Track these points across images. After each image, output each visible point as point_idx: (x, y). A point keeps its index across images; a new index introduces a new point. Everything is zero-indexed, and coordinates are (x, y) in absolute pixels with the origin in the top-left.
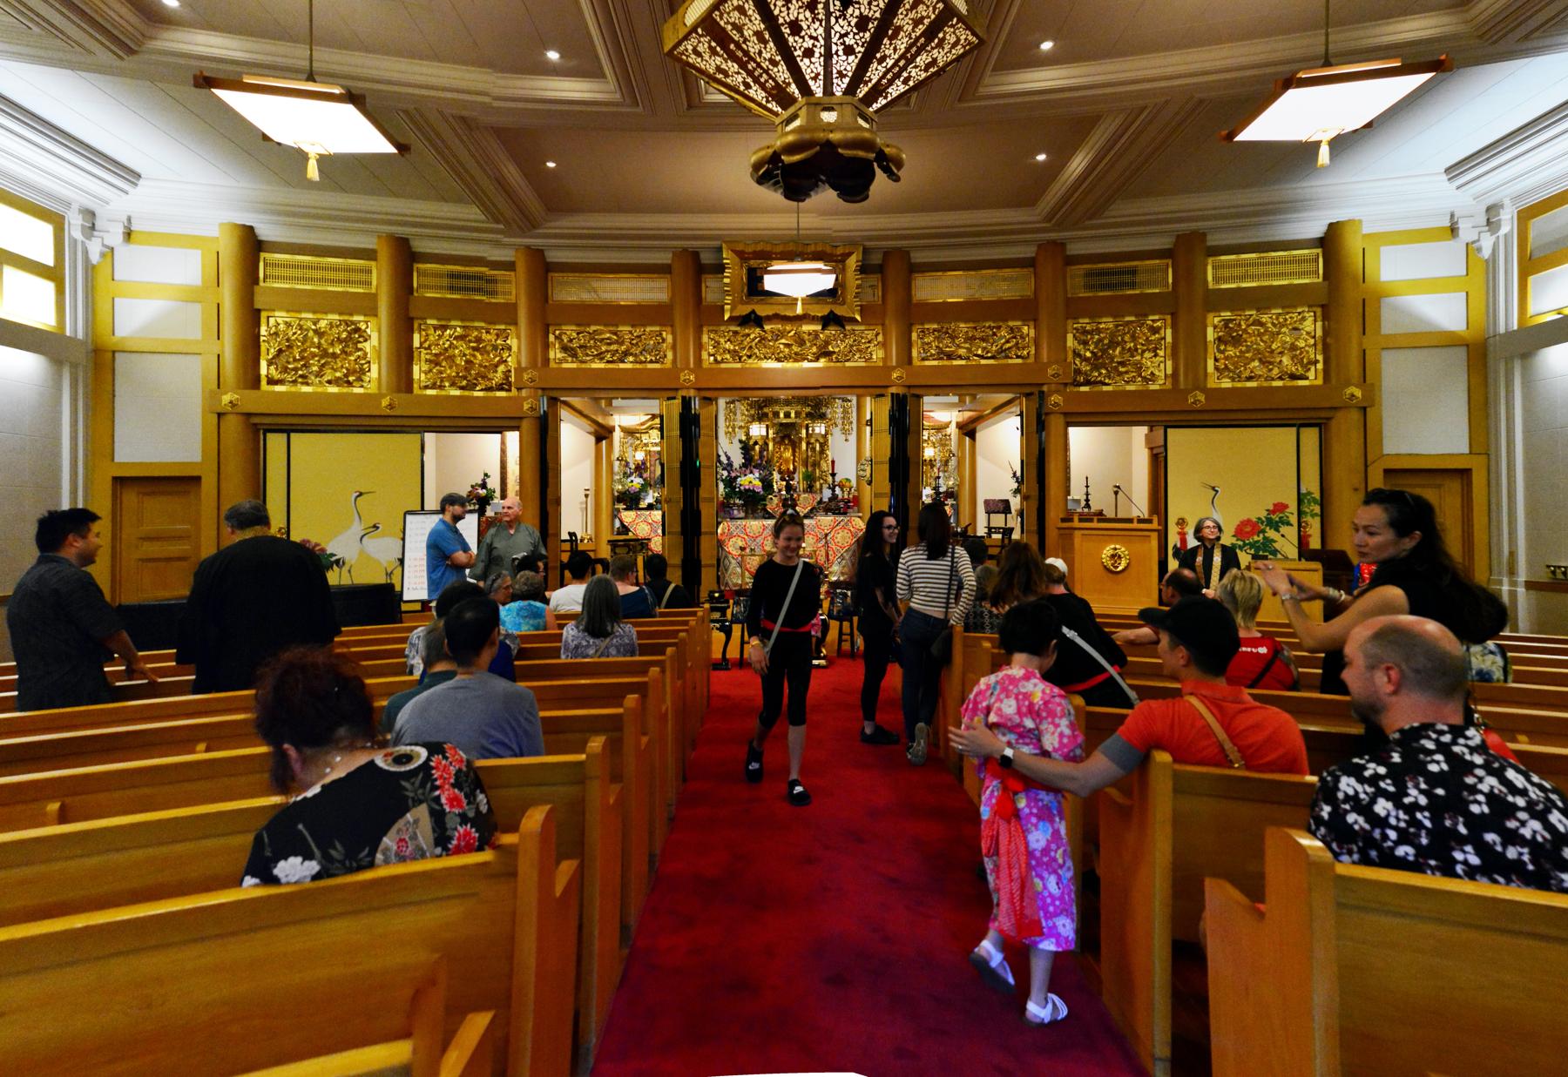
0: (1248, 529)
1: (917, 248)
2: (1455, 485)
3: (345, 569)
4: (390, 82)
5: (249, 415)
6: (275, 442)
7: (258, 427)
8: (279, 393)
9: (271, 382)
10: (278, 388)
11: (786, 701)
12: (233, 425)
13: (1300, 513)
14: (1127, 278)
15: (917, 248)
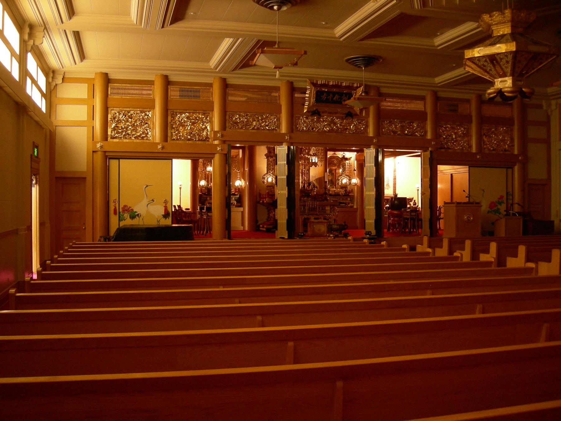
1: (385, 87)
2: (229, 91)
3: (141, 218)
4: (453, 78)
5: (105, 152)
6: (114, 164)
7: (108, 157)
9: (113, 138)
10: (115, 140)
11: (177, 225)
12: (99, 157)
13: (507, 199)
14: (185, 93)
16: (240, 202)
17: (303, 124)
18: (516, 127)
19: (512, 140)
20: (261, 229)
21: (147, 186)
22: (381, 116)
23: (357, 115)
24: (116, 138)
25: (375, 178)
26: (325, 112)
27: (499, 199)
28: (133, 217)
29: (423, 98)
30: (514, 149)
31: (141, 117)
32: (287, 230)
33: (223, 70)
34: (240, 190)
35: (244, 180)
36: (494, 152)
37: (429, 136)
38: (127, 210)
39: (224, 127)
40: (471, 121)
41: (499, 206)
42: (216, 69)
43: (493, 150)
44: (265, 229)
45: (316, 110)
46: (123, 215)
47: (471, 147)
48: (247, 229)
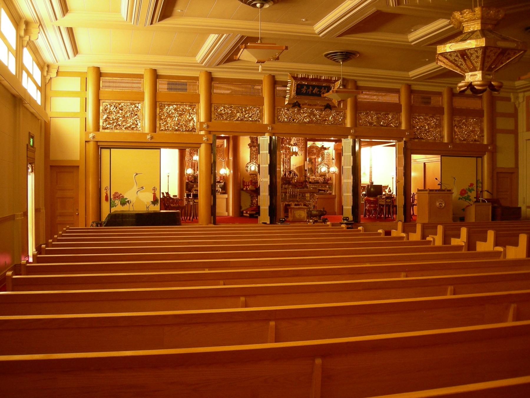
0: (463, 192)
3: (131, 204)
5: (97, 142)
6: (105, 153)
7: (99, 147)
8: (105, 135)
9: (104, 128)
10: (106, 131)
12: (91, 147)
13: (477, 187)
14: (183, 87)
15: (360, 80)
16: (225, 189)
17: (284, 115)
18: (485, 119)
19: (482, 131)
20: (245, 215)
21: (137, 174)
22: (357, 108)
23: (335, 107)
24: (107, 128)
25: (352, 167)
26: (305, 104)
27: (470, 186)
28: (123, 204)
29: (397, 91)
30: (483, 140)
31: (131, 109)
32: (269, 215)
33: (209, 65)
34: (225, 179)
35: (229, 168)
36: (464, 142)
37: (403, 127)
38: (117, 197)
39: (209, 118)
40: (443, 113)
41: (469, 193)
42: (202, 63)
43: (464, 140)
44: (248, 215)
45: (297, 102)
46: (114, 202)
47: (442, 137)
48: (231, 214)
